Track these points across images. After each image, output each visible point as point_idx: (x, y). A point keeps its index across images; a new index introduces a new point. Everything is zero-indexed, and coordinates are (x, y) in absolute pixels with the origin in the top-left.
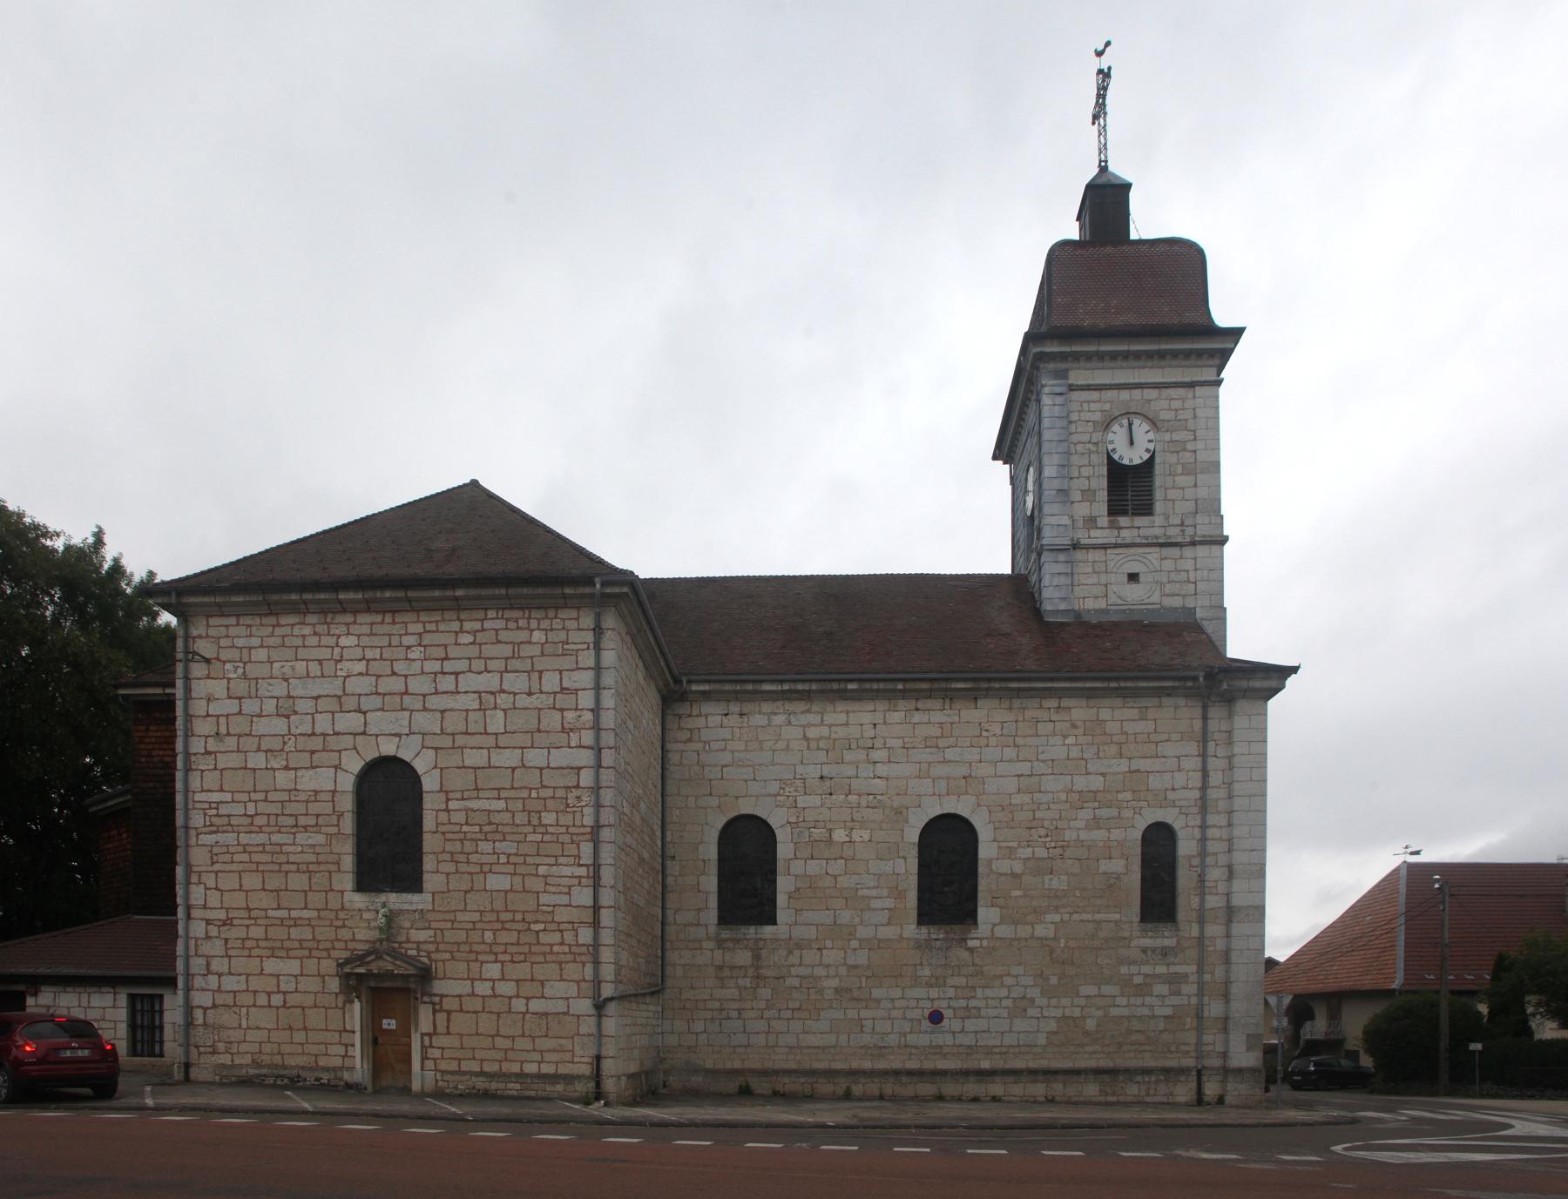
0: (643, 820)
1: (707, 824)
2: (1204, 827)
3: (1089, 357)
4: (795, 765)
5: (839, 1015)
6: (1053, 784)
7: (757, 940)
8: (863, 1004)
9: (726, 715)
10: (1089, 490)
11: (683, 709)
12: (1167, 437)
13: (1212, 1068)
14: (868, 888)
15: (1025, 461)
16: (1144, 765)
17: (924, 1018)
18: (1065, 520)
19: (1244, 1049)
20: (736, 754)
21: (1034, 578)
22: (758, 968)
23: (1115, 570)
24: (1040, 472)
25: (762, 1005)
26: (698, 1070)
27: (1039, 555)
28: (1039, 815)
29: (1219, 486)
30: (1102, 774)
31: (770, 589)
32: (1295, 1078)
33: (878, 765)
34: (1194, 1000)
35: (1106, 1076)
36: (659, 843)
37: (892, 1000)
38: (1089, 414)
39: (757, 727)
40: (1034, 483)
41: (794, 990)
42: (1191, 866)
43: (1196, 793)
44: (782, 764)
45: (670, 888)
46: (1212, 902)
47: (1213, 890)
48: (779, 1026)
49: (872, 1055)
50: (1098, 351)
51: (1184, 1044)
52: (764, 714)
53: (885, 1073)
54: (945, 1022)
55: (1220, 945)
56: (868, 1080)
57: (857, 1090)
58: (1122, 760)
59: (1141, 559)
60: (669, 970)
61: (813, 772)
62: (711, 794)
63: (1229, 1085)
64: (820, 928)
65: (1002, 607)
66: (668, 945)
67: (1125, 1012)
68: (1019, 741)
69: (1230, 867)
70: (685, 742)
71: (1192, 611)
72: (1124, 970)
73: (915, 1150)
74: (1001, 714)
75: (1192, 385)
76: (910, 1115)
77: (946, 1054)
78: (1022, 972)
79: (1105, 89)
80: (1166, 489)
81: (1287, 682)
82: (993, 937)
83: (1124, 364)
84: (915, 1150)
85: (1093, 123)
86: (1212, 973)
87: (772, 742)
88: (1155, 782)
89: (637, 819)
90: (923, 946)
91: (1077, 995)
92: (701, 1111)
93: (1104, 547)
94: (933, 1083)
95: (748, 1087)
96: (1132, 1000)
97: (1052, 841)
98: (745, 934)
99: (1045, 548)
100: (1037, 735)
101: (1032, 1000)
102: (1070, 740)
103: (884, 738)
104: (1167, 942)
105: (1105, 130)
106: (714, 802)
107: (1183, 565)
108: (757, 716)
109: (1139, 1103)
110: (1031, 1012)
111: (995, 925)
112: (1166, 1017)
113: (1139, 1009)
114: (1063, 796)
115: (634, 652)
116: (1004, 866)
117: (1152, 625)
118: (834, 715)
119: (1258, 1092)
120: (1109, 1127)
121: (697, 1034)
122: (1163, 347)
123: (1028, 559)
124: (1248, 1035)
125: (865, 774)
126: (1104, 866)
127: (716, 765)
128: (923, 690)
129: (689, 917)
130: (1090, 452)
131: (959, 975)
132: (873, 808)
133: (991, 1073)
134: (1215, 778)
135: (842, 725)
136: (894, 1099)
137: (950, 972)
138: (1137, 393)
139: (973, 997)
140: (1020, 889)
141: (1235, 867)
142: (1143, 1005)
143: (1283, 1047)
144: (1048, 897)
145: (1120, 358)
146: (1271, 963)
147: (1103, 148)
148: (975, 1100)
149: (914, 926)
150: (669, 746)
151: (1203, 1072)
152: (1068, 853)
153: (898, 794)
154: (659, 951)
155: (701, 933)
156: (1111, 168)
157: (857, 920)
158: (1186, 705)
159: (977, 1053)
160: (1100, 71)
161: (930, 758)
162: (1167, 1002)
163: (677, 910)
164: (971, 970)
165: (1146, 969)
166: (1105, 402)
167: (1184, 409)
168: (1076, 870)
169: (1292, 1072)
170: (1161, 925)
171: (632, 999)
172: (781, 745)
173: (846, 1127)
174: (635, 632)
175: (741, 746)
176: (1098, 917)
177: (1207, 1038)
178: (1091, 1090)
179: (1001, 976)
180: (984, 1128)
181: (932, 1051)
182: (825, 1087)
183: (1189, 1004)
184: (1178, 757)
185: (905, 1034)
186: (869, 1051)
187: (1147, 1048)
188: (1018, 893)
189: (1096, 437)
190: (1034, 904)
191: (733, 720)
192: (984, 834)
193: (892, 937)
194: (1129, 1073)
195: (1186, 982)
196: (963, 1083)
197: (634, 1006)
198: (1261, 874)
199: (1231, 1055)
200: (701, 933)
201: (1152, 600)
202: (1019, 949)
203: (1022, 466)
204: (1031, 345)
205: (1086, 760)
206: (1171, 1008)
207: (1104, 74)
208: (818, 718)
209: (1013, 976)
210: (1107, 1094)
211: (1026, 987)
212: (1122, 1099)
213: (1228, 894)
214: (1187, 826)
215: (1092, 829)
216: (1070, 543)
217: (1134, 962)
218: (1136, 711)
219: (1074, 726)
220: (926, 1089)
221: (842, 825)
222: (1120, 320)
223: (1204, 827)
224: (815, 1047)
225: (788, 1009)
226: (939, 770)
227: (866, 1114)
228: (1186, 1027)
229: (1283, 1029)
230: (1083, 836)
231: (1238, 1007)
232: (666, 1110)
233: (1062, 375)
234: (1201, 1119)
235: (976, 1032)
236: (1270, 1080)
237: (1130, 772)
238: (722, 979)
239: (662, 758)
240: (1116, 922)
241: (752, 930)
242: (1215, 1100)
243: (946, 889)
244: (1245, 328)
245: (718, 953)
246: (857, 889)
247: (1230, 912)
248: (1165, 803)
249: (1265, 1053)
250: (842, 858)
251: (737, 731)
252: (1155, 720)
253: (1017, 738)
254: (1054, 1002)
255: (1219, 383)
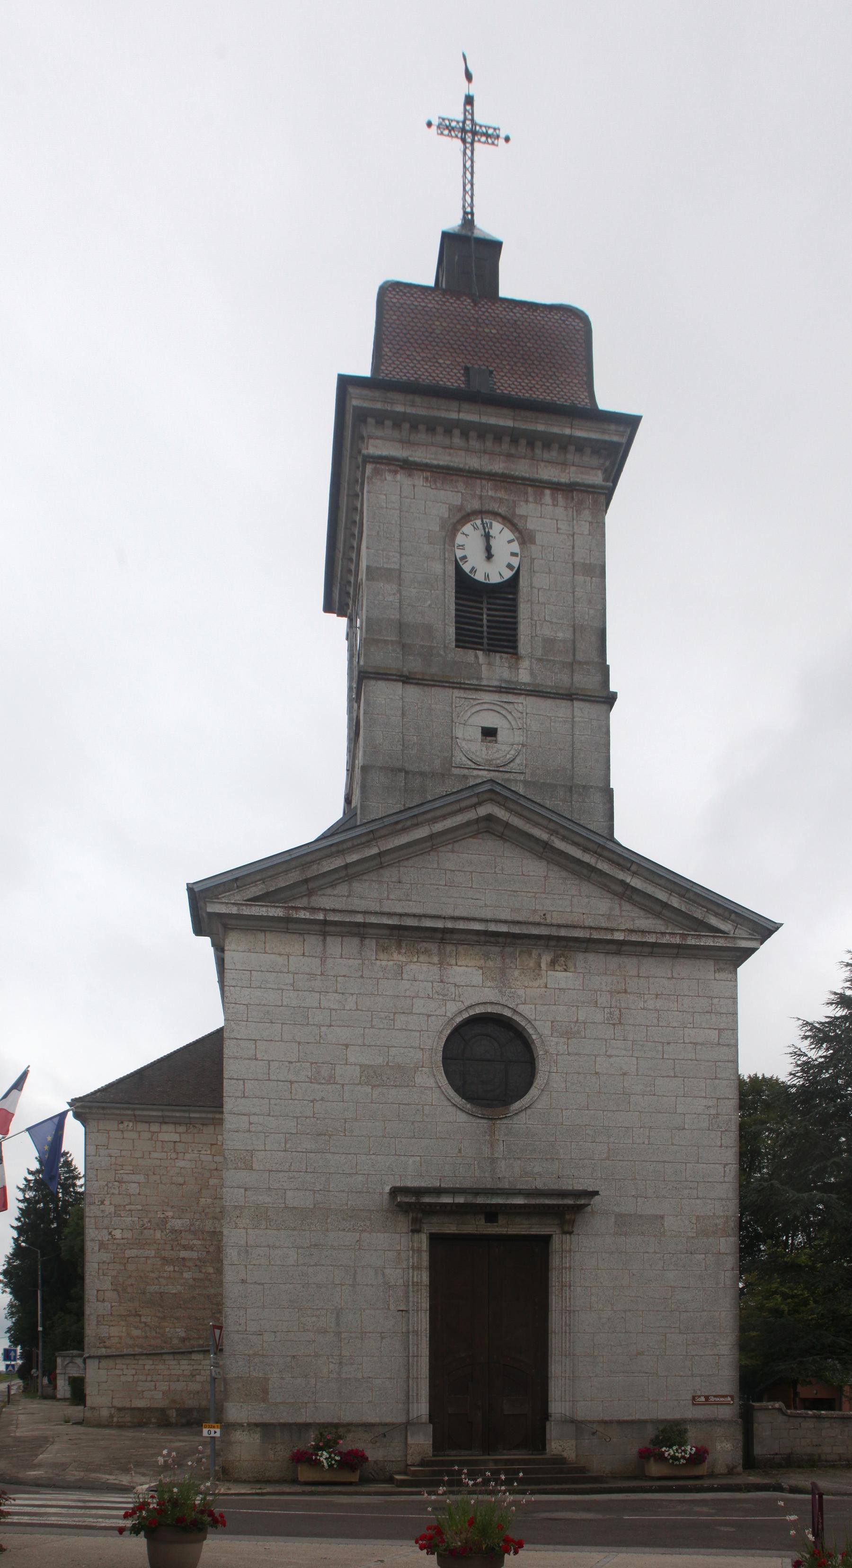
156: (478, 222)
244: (776, 927)
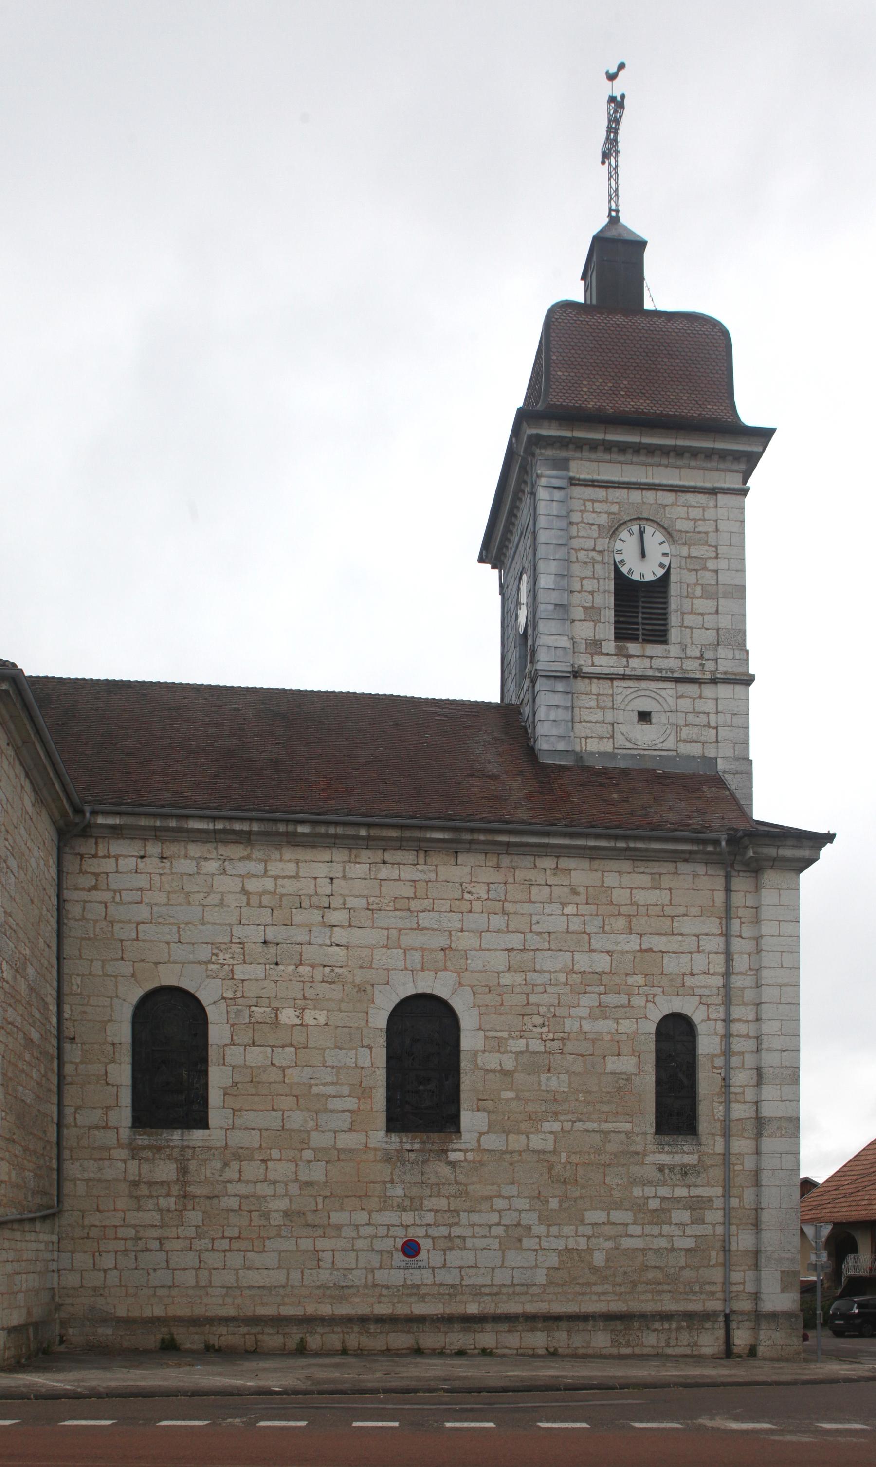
0: (32, 989)
1: (117, 997)
2: (728, 1021)
3: (594, 446)
4: (231, 925)
5: (290, 1245)
6: (551, 962)
7: (183, 1148)
8: (320, 1232)
9: (142, 857)
10: (593, 607)
11: (86, 847)
12: (685, 551)
13: (742, 1313)
14: (324, 1084)
15: (517, 567)
16: (658, 943)
17: (397, 1250)
18: (564, 642)
19: (778, 1290)
20: (155, 908)
21: (527, 710)
22: (185, 1184)
23: (622, 707)
24: (534, 581)
25: (191, 1232)
26: (106, 1319)
27: (533, 682)
28: (533, 999)
29: (744, 615)
30: (608, 952)
31: (201, 701)
32: (837, 1322)
33: (336, 929)
34: (720, 1230)
35: (619, 1322)
36: (54, 1020)
37: (357, 1226)
38: (594, 515)
39: (182, 875)
40: (528, 594)
41: (231, 1214)
42: (714, 1067)
43: (719, 981)
44: (213, 924)
45: (69, 1079)
46: (739, 1111)
47: (739, 1097)
48: (213, 1259)
49: (331, 1297)
50: (604, 440)
51: (709, 1283)
52: (192, 858)
53: (348, 1320)
54: (423, 1255)
55: (749, 1163)
56: (327, 1329)
57: (314, 1342)
58: (633, 937)
59: (653, 695)
60: (68, 1187)
61: (255, 935)
62: (122, 959)
63: (762, 1332)
64: (265, 1133)
65: (489, 743)
66: (66, 1154)
67: (639, 1243)
68: (509, 907)
69: (759, 1070)
70: (89, 891)
71: (712, 762)
72: (637, 1192)
73: (380, 1424)
74: (488, 874)
75: (713, 492)
76: (379, 1375)
77: (424, 1296)
78: (515, 1193)
79: (618, 121)
80: (683, 613)
81: (821, 852)
82: (479, 1149)
83: (635, 459)
84: (380, 1424)
85: (603, 163)
86: (740, 1198)
87: (202, 895)
88: (671, 964)
89: (23, 987)
90: (389, 1158)
91: (582, 1222)
92: (108, 1375)
93: (611, 678)
94: (409, 1332)
95: (173, 1339)
96: (648, 1229)
97: (549, 1032)
98: (167, 1140)
99: (541, 673)
100: (531, 902)
101: (529, 1228)
102: (570, 909)
103: (343, 896)
104: (691, 1159)
105: (616, 173)
106: (126, 968)
107: (701, 705)
108: (182, 861)
109: (657, 1355)
110: (527, 1243)
111: (481, 1134)
112: (688, 1250)
113: (655, 1240)
114: (562, 977)
115: (19, 769)
116: (492, 1061)
117: (666, 776)
118: (280, 865)
119: (796, 1342)
120: (622, 1387)
121: (105, 1271)
122: (681, 442)
123: (520, 687)
124: (782, 1272)
125: (319, 941)
126: (613, 1064)
127: (130, 922)
128: (390, 839)
129: (95, 1117)
130: (594, 562)
131: (438, 1196)
132: (330, 983)
133: (480, 1320)
134: (741, 963)
135: (290, 877)
136: (360, 1353)
137: (428, 1192)
138: (650, 496)
139: (457, 1224)
140: (511, 1089)
141: (765, 1071)
142: (660, 1235)
143: (822, 1285)
144: (546, 1101)
145: (630, 451)
146: (807, 1185)
147: (614, 194)
148: (461, 1353)
149: (382, 1133)
150: (67, 894)
151: (731, 1318)
152: (569, 1047)
153: (361, 967)
154: (54, 1162)
155: (109, 1138)
156: (623, 220)
157: (311, 1124)
158: (706, 874)
159: (462, 1294)
160: (612, 99)
161: (401, 924)
162: (689, 1232)
163: (78, 1108)
164: (453, 1189)
165: (663, 1191)
166: (612, 503)
167: (704, 520)
168: (579, 1067)
169: (834, 1314)
170: (680, 1138)
171: (16, 1226)
172: (213, 899)
173: (296, 1392)
174: (20, 743)
175: (162, 898)
176: (607, 1126)
177: (736, 1276)
178: (601, 1340)
179: (490, 1198)
180: (470, 1391)
181: (406, 1292)
182: (272, 1339)
183: (714, 1235)
184: (698, 936)
185: (372, 1270)
186: (328, 1292)
187: (666, 1287)
188: (510, 1094)
189: (603, 543)
190: (530, 1108)
191: (152, 865)
192: (468, 1021)
193: (353, 1147)
194: (645, 1318)
195: (711, 1208)
196: (446, 1333)
197: (18, 1235)
198: (794, 1079)
199: (763, 1296)
200: (109, 1138)
201: (666, 745)
202: (511, 1164)
203: (514, 573)
204: (525, 425)
205: (589, 934)
206: (694, 1240)
207: (617, 104)
208: (261, 867)
209: (504, 1197)
210: (619, 1345)
211: (520, 1211)
212: (637, 1350)
213: (757, 1102)
214: (709, 1019)
215: (597, 1019)
216: (569, 669)
217: (650, 1183)
218: (647, 878)
219: (575, 892)
220: (401, 1340)
221: (292, 1003)
222: (629, 406)
223: (728, 1021)
224: (259, 1287)
225: (223, 1237)
226: (411, 939)
227: (321, 1374)
228: (711, 1263)
229: (822, 1265)
230: (586, 1027)
231: (771, 1239)
232: (60, 1376)
233: (562, 465)
234: (730, 1376)
235: (461, 1268)
236: (809, 1324)
237: (641, 951)
238: (138, 1198)
239: (58, 910)
240: (627, 1133)
241: (176, 1135)
242: (747, 1351)
243: (421, 1088)
245: (133, 1165)
246: (311, 1086)
247: (760, 1124)
248: (682, 990)
249: (801, 1293)
250: (292, 1045)
251: (156, 878)
252: (670, 889)
253: (506, 904)
254: (554, 1230)
255: (745, 492)
